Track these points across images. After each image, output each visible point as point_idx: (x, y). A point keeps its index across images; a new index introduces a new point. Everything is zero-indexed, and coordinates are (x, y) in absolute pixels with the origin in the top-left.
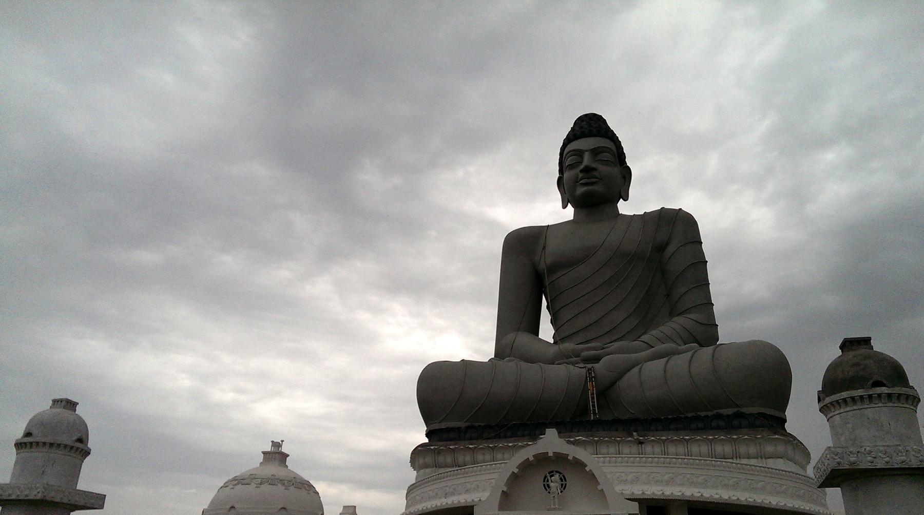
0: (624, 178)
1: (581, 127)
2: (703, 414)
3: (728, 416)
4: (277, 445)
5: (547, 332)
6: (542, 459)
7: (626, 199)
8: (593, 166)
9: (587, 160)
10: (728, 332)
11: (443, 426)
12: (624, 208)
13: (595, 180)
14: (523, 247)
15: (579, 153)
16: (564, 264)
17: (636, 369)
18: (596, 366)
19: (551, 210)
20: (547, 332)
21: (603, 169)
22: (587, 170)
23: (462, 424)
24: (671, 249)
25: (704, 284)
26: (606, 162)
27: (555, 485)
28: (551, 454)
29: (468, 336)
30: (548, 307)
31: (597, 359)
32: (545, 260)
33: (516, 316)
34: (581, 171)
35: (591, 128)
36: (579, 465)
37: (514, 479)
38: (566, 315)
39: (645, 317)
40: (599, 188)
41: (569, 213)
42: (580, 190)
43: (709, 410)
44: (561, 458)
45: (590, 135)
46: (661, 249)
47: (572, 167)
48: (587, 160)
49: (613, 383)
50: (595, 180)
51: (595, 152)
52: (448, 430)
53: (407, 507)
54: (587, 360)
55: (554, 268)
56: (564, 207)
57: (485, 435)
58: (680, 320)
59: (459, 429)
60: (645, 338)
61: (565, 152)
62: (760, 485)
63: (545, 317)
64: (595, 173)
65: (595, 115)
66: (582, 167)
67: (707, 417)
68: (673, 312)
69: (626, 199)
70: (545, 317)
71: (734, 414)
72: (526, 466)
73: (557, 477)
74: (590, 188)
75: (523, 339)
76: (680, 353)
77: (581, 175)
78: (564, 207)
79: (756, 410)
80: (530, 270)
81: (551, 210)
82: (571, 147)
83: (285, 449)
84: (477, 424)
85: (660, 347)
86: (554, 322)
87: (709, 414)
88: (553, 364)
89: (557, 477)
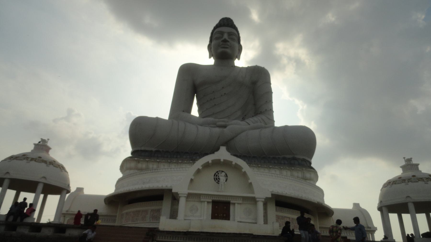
3: (289, 159)
4: (43, 141)
5: (195, 111)
6: (216, 163)
7: (239, 59)
9: (226, 36)
11: (143, 148)
14: (188, 72)
15: (222, 33)
18: (225, 130)
20: (195, 111)
22: (225, 41)
23: (154, 149)
27: (222, 179)
28: (222, 160)
31: (225, 127)
33: (180, 104)
36: (237, 168)
40: (228, 51)
41: (211, 62)
42: (220, 50)
44: (227, 164)
48: (226, 36)
49: (233, 138)
51: (230, 34)
53: (115, 190)
54: (220, 126)
56: (210, 57)
59: (151, 151)
60: (247, 121)
61: (214, 32)
64: (228, 43)
65: (230, 18)
69: (239, 59)
72: (206, 166)
73: (223, 174)
74: (224, 49)
77: (221, 43)
78: (210, 57)
80: (191, 81)
83: (49, 144)
89: (223, 174)
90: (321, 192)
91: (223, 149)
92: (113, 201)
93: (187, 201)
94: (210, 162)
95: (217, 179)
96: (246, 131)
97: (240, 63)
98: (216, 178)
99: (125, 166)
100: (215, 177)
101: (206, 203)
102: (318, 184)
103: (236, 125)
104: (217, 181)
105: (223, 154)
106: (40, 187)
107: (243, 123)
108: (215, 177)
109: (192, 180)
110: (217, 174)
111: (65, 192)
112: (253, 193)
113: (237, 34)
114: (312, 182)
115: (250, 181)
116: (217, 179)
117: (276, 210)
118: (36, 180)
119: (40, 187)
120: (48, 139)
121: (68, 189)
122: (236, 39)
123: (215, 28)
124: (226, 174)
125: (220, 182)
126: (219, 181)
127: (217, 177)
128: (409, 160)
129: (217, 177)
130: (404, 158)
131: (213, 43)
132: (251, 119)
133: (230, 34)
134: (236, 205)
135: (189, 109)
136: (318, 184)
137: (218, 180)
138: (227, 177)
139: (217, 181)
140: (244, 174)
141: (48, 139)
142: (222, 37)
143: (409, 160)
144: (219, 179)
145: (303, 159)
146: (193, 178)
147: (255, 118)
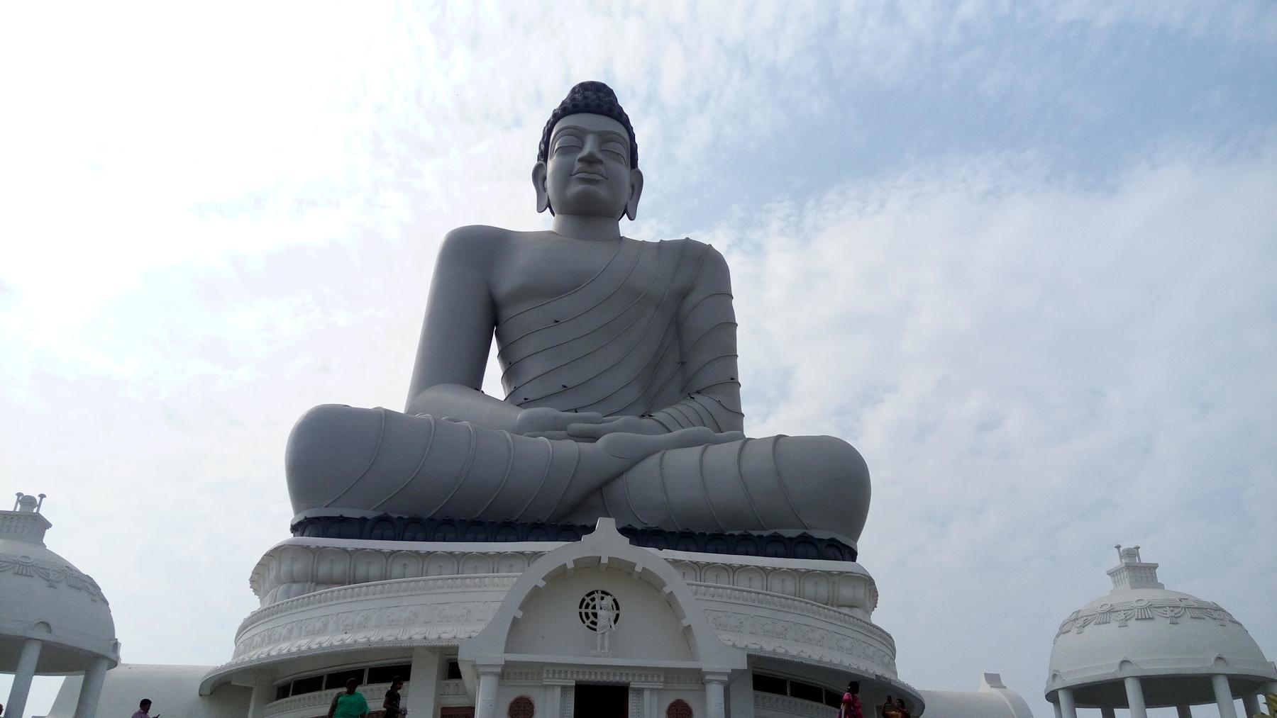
0: (633, 187)
1: (585, 98)
2: (755, 533)
3: (791, 539)
4: (27, 502)
6: (590, 565)
8: (600, 156)
9: (589, 147)
10: (756, 427)
12: (626, 227)
16: (541, 290)
17: (655, 459)
19: (523, 213)
21: (610, 164)
22: (590, 161)
23: (370, 514)
24: (694, 298)
25: (730, 355)
27: (604, 616)
29: (381, 373)
30: (503, 355)
31: (593, 437)
32: (508, 281)
33: (448, 361)
34: (581, 160)
36: (649, 582)
37: (534, 599)
40: (601, 191)
41: (546, 222)
42: (575, 189)
43: (764, 529)
44: (620, 569)
46: (683, 294)
48: (589, 147)
49: (619, 475)
52: (342, 520)
53: (237, 654)
55: (525, 293)
59: (364, 519)
60: (659, 415)
62: (847, 644)
63: (494, 369)
64: (600, 167)
65: (604, 86)
67: (761, 537)
70: (494, 369)
71: (801, 536)
72: (559, 576)
73: (608, 601)
74: (592, 188)
75: (453, 399)
77: (578, 166)
78: (540, 210)
79: (824, 535)
80: (481, 293)
81: (523, 213)
87: (765, 534)
89: (608, 601)
90: (886, 641)
91: (606, 527)
92: (223, 687)
93: (500, 685)
94: (570, 566)
95: (589, 618)
96: (681, 469)
97: (640, 228)
98: (587, 614)
99: (274, 571)
100: (583, 610)
101: (558, 691)
102: (877, 618)
103: (618, 435)
104: (588, 622)
105: (606, 539)
106: (31, 655)
107: (646, 421)
108: (583, 610)
109: (515, 621)
110: (588, 600)
111: (106, 664)
112: (692, 655)
113: (626, 136)
114: (858, 613)
115: (685, 623)
116: (588, 618)
117: (756, 704)
118: (19, 633)
119: (31, 655)
120: (42, 496)
121: (112, 656)
122: (625, 153)
123: (557, 117)
124: (615, 600)
125: (597, 627)
126: (595, 623)
127: (590, 611)
128: (1133, 553)
129: (590, 611)
130: (1118, 547)
131: (551, 165)
132: (669, 410)
133: (604, 138)
134: (647, 694)
135: (474, 380)
136: (877, 618)
137: (592, 618)
138: (618, 608)
139: (588, 622)
140: (670, 602)
141: (42, 496)
142: (581, 148)
143: (1133, 553)
144: (595, 615)
145: (833, 540)
146: (519, 614)
147: (683, 409)
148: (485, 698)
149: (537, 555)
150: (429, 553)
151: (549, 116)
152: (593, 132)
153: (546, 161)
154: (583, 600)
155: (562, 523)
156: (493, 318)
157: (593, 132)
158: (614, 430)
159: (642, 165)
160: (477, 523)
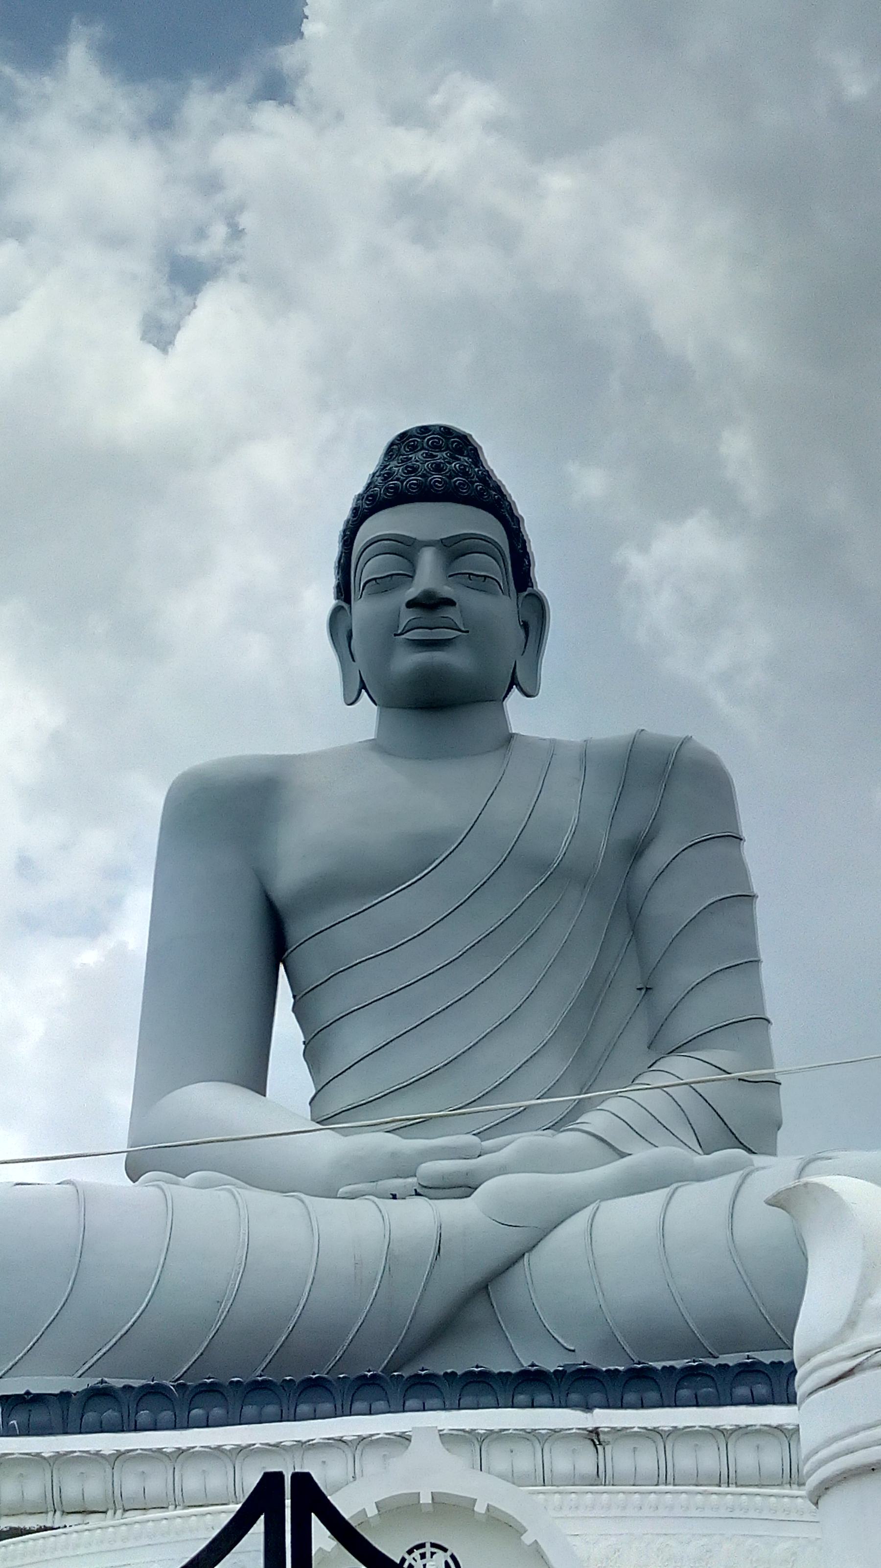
0: (525, 626)
8: (446, 591)
9: (428, 574)
13: (451, 634)
15: (405, 549)
16: (360, 883)
17: (580, 1221)
21: (472, 601)
22: (429, 603)
23: (76, 1385)
24: (658, 856)
26: (480, 582)
30: (296, 1009)
31: (462, 1187)
34: (411, 604)
35: (433, 468)
38: (355, 1040)
39: (590, 1057)
40: (456, 660)
42: (408, 661)
45: (425, 494)
46: (636, 850)
47: (383, 585)
48: (428, 562)
50: (451, 634)
51: (453, 549)
55: (328, 890)
57: (408, 1404)
58: (681, 1067)
59: (65, 1396)
64: (451, 613)
66: (413, 592)
68: (661, 1045)
74: (438, 657)
75: (214, 1103)
76: (700, 1176)
77: (407, 616)
82: (378, 525)
84: (118, 1383)
85: (641, 1156)
86: (314, 1052)
88: (331, 1194)
97: (559, 710)
103: (516, 1175)
107: (566, 1138)
110: (428, 1550)
123: (360, 515)
132: (612, 1104)
135: (255, 1079)
148: (406, 1565)
149: (404, 1438)
150: (180, 1452)
151: (345, 513)
152: (428, 544)
153: (348, 600)
154: (422, 1546)
155: (406, 1373)
156: (276, 938)
157: (428, 544)
158: (503, 1170)
159: (543, 578)
160: (259, 1387)
